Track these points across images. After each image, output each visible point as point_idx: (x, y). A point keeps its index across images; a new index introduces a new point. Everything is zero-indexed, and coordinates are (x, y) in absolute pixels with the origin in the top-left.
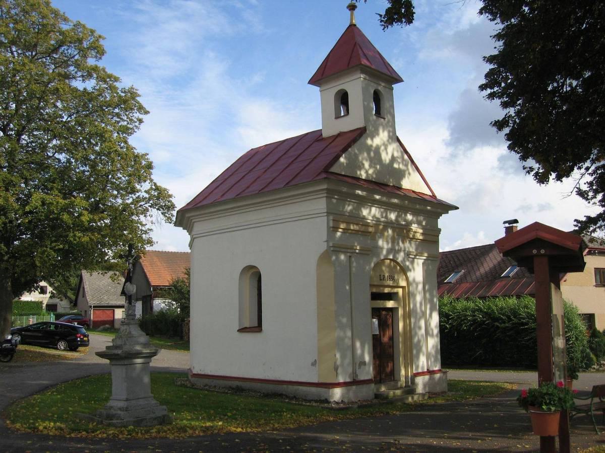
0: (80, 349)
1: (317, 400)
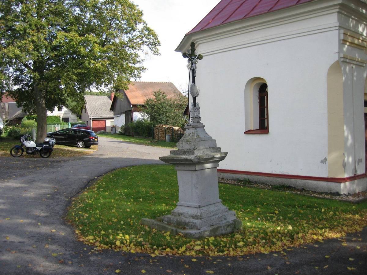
0: (92, 146)
1: (327, 192)
